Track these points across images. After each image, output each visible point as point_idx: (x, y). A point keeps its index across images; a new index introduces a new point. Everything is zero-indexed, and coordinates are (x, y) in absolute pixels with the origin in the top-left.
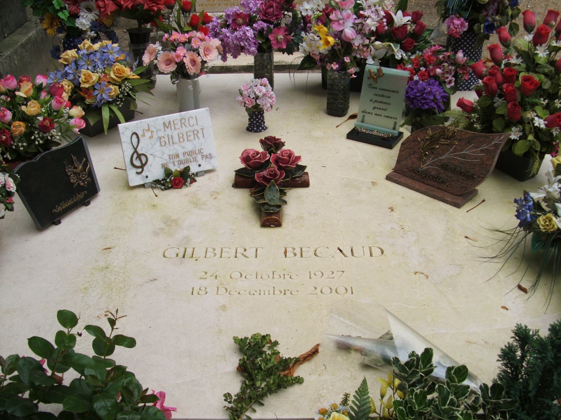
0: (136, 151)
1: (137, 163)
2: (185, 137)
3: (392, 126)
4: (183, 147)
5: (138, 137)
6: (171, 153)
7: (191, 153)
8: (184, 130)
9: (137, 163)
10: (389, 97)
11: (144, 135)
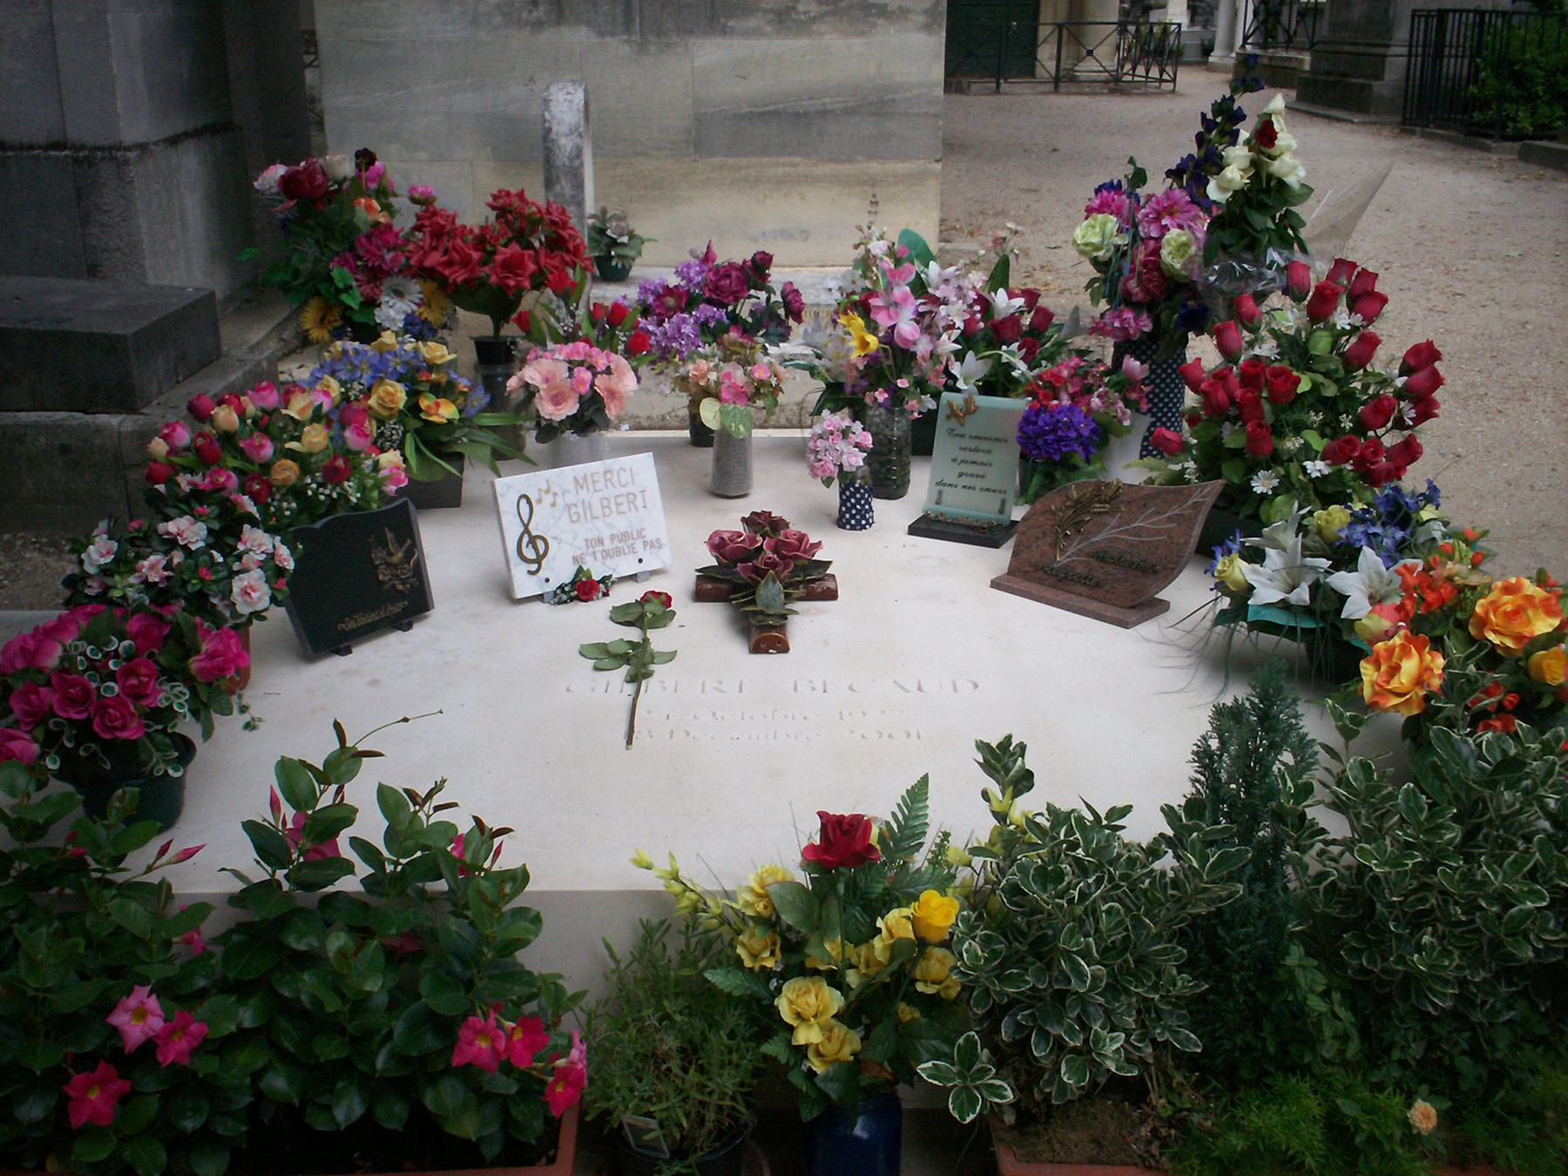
0: (526, 531)
1: (530, 553)
2: (613, 506)
3: (997, 506)
4: (610, 526)
5: (529, 502)
6: (590, 536)
7: (625, 536)
8: (611, 492)
9: (530, 553)
10: (989, 452)
11: (539, 501)
